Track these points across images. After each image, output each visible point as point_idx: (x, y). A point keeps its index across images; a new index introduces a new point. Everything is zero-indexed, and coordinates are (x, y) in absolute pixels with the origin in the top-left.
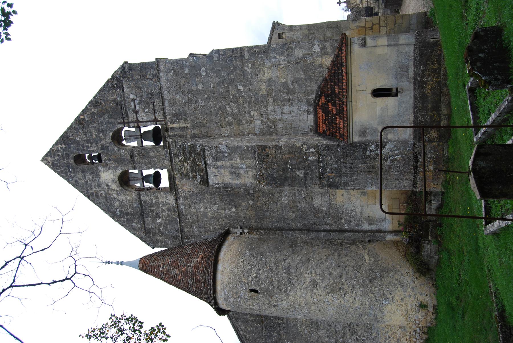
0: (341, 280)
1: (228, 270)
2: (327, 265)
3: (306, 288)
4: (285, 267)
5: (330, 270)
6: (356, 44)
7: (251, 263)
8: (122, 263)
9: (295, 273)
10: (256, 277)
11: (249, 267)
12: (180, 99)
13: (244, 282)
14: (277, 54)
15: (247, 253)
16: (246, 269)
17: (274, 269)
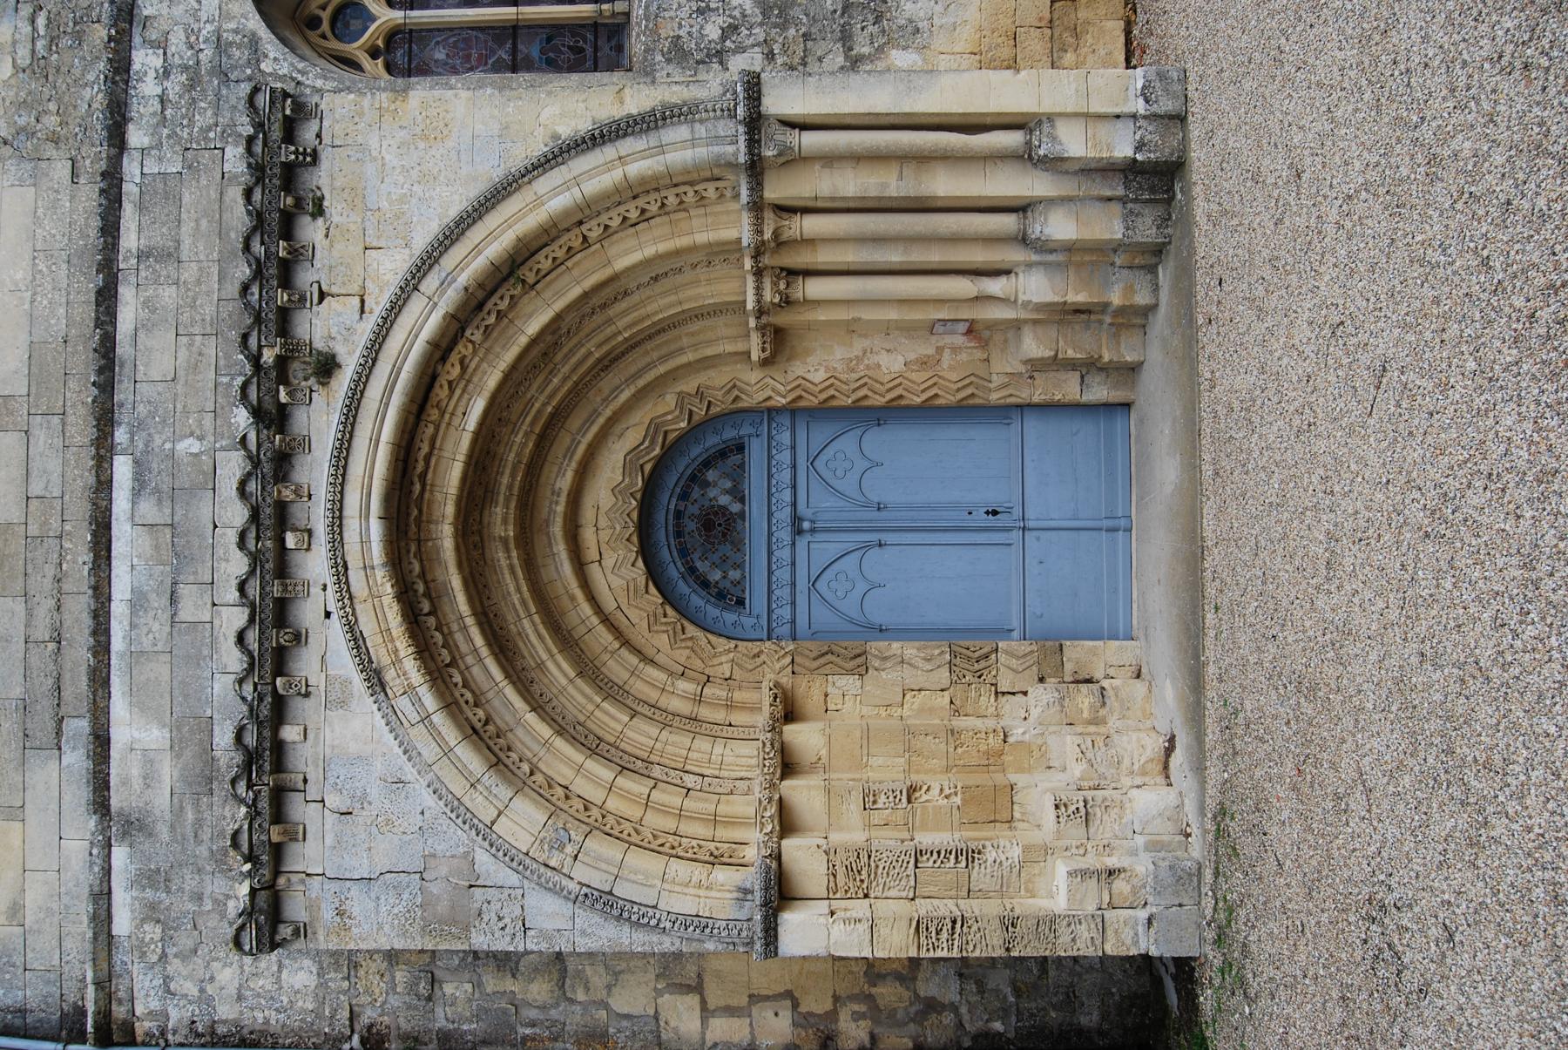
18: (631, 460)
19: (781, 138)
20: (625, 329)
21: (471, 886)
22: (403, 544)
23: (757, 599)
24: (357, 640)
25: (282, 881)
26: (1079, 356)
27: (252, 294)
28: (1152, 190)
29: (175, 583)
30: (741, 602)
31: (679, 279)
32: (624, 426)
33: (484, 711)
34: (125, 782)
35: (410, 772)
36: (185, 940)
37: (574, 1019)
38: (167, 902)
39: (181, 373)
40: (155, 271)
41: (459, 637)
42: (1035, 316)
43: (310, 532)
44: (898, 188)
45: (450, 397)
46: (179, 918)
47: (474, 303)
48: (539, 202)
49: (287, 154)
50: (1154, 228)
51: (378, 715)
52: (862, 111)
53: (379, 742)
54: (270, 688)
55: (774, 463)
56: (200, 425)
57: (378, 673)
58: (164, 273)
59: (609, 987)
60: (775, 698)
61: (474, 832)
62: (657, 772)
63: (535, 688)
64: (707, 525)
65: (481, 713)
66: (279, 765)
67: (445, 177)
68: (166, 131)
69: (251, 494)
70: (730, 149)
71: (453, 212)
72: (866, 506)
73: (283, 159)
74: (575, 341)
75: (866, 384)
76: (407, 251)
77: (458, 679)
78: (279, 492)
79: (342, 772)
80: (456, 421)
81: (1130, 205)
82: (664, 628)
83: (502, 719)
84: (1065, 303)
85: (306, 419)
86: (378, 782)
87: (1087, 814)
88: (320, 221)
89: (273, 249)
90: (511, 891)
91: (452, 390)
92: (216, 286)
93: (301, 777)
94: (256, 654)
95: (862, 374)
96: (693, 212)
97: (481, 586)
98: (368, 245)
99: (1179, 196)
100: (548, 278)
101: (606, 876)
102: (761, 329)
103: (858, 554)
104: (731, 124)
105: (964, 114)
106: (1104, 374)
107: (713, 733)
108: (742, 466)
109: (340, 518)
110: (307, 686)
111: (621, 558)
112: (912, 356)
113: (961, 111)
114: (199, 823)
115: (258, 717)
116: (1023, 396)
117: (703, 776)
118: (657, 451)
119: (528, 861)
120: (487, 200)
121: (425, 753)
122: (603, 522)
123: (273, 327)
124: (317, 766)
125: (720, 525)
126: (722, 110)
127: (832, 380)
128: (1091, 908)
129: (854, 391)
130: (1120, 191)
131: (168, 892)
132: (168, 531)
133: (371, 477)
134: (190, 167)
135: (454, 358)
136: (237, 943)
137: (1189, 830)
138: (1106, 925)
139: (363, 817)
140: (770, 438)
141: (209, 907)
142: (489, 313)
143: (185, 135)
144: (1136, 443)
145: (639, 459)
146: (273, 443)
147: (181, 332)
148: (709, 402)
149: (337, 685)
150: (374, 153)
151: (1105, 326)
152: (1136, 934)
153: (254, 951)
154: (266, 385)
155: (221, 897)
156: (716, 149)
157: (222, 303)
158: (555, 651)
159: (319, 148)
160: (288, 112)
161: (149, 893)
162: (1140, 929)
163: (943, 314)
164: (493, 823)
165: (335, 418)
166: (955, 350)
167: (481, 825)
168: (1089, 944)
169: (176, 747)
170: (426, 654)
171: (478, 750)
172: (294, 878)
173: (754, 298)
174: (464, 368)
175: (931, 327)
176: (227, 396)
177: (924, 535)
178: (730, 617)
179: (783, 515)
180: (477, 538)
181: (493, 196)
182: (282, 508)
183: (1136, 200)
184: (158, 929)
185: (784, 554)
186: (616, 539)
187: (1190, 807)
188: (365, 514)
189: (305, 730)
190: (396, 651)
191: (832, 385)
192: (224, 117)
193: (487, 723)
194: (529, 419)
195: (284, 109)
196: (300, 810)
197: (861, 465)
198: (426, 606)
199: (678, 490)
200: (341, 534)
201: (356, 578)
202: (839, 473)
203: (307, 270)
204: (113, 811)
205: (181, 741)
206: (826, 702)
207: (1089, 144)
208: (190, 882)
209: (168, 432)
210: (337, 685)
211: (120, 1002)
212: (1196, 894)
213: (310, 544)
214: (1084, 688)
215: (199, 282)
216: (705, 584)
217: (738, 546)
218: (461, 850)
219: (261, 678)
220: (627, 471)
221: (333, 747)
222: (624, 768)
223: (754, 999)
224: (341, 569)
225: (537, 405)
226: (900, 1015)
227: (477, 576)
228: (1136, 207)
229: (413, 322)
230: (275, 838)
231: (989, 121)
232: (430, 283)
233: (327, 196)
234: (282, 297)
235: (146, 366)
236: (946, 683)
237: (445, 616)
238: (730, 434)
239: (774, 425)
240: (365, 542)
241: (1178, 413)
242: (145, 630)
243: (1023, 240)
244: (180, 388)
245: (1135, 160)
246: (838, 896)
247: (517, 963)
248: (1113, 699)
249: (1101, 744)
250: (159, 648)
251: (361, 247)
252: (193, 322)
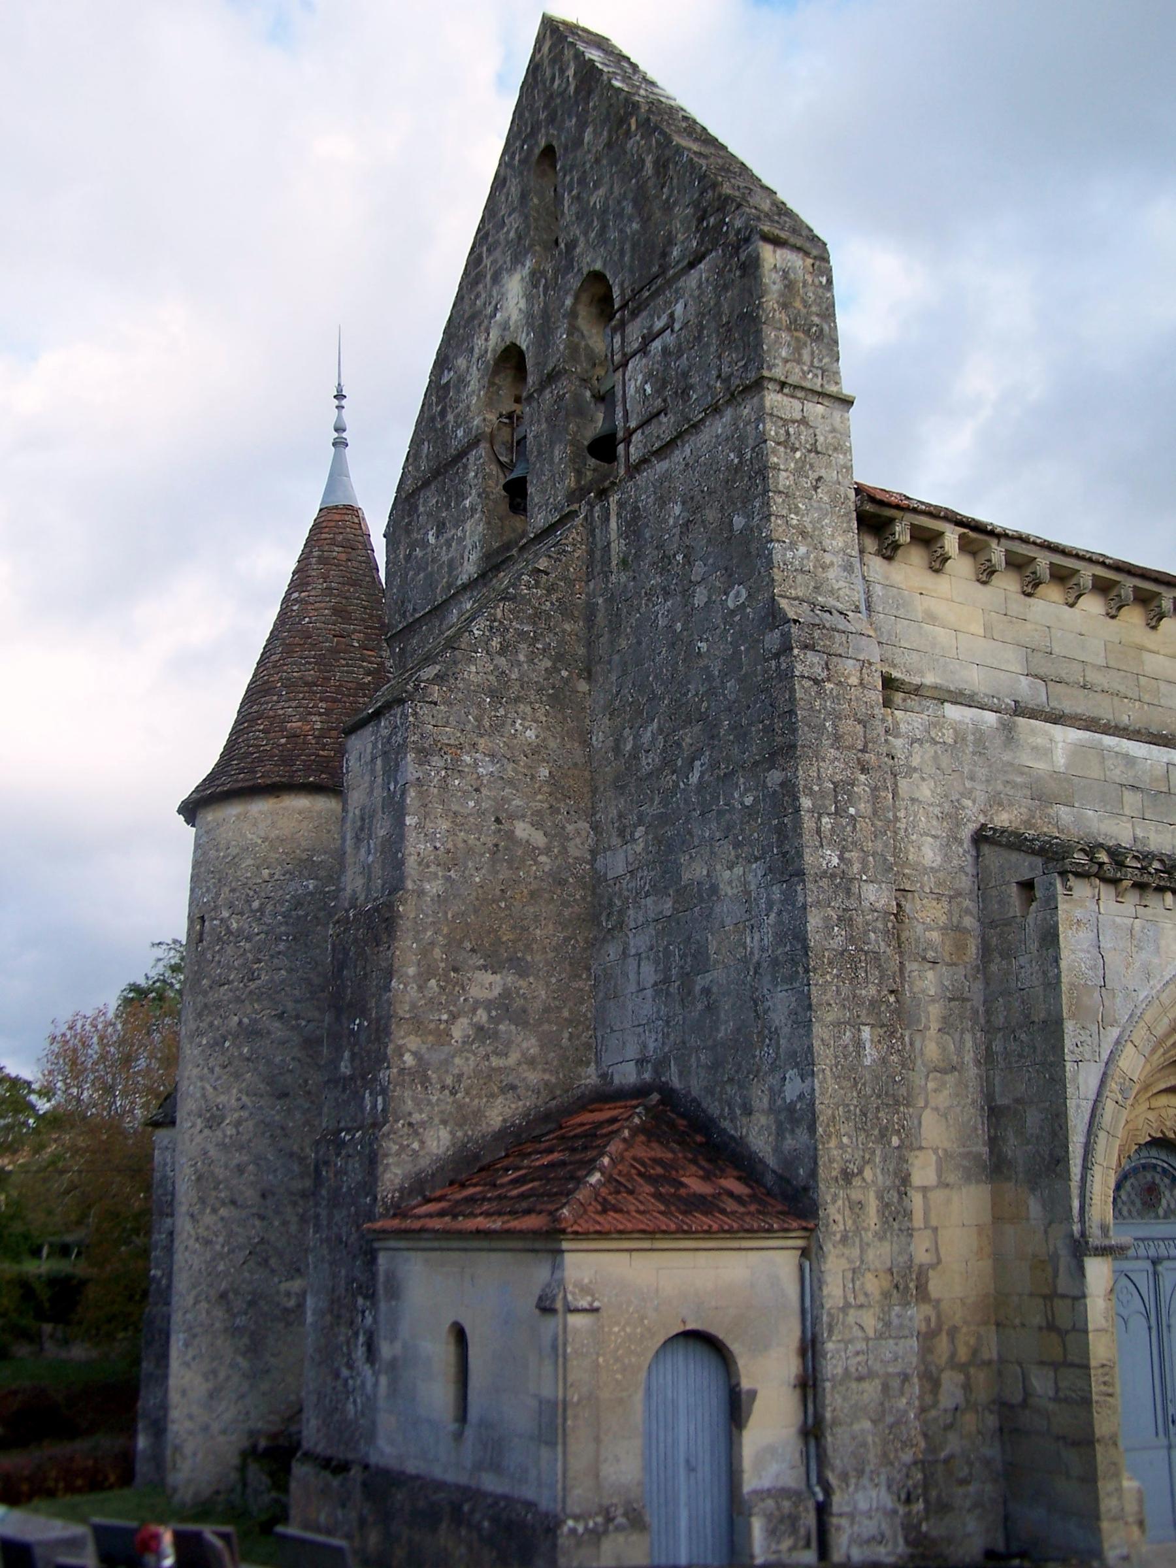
0: (223, 1204)
1: (249, 836)
2: (266, 1159)
3: (204, 1096)
4: (256, 1020)
5: (251, 1167)
6: (553, 1273)
7: (269, 908)
8: (340, 444)
9: (241, 1054)
10: (229, 932)
11: (256, 905)
12: (671, 521)
13: (218, 895)
14: (780, 913)
15: (307, 887)
16: (251, 893)
17: (252, 985)
34: (1033, 731)
37: (917, 1079)
59: (936, 1109)
114: (1015, 786)
161: (971, 738)
204: (1016, 718)
211: (904, 700)
223: (935, 1230)
226: (929, 1358)
247: (948, 1034)
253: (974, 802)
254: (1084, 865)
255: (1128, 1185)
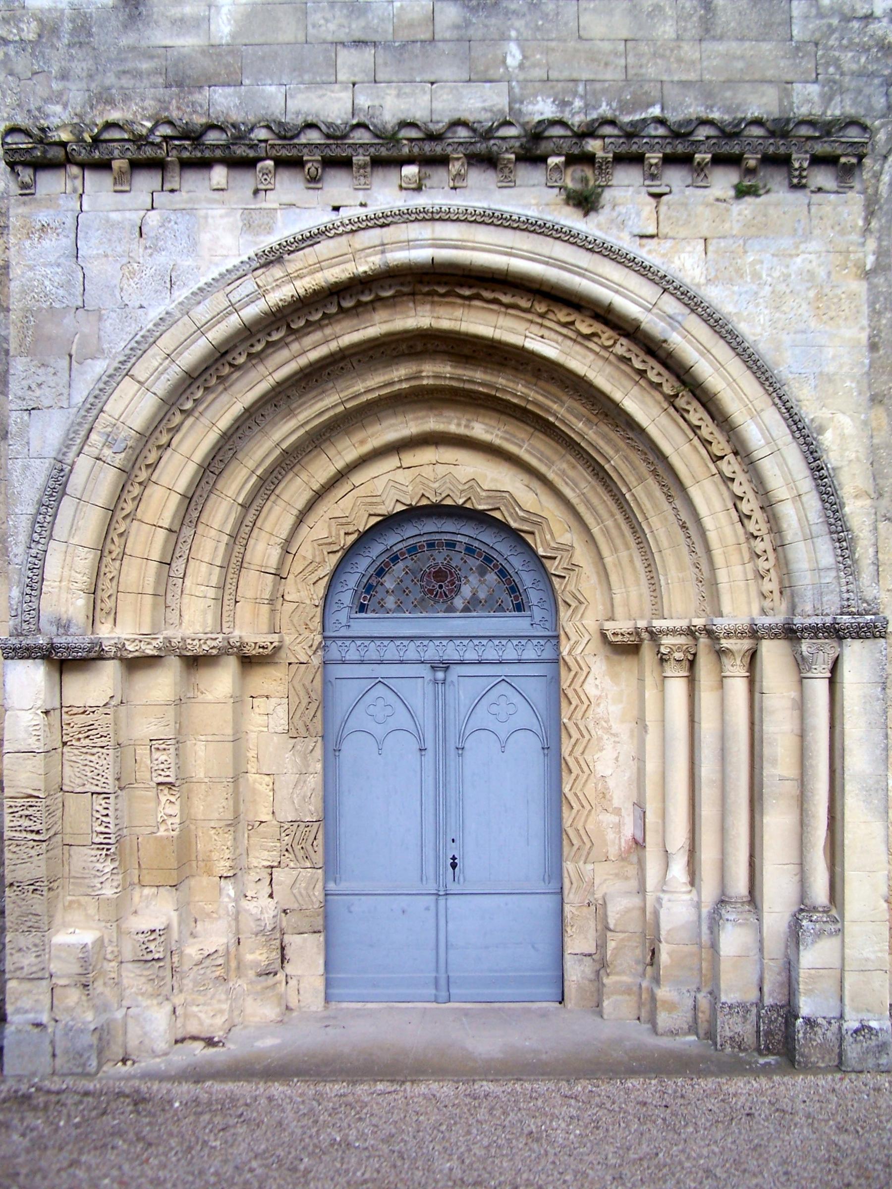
18: (503, 498)
19: (820, 660)
20: (633, 495)
21: (71, 356)
22: (409, 279)
23: (365, 625)
24: (310, 239)
25: (75, 170)
26: (609, 953)
27: (656, 129)
28: (768, 1033)
29: (375, 44)
30: (362, 608)
31: (685, 550)
32: (538, 492)
33: (244, 363)
35: (182, 294)
36: (21, 64)
38: (59, 45)
39: (587, 45)
40: (691, 16)
41: (317, 336)
42: (649, 910)
43: (419, 189)
44: (773, 776)
45: (559, 323)
46: (44, 57)
47: (652, 346)
48: (755, 415)
49: (800, 160)
50: (731, 1034)
51: (236, 261)
52: (846, 743)
53: (211, 262)
54: (263, 155)
55: (504, 642)
56: (534, 65)
57: (279, 260)
58: (689, 26)
60: (263, 647)
61: (122, 358)
62: (187, 532)
63: (269, 409)
64: (440, 575)
65: (241, 360)
66: (186, 165)
67: (779, 319)
68: (835, 22)
69: (455, 132)
70: (809, 608)
71: (743, 328)
72: (462, 737)
73: (794, 156)
74: (622, 444)
75: (583, 736)
76: (703, 281)
77: (275, 337)
78: (458, 159)
79: (182, 227)
80: (535, 329)
81: (754, 1010)
82: (334, 534)
83: (237, 379)
84: (660, 941)
85: (531, 182)
86: (172, 263)
87: (146, 961)
88: (732, 193)
89: (702, 148)
90: (66, 395)
91: (565, 325)
92: (676, 78)
93: (176, 187)
94: (296, 141)
95: (593, 732)
96: (749, 567)
97: (371, 353)
98: (709, 241)
99: (762, 1061)
100: (681, 421)
101: (80, 488)
102: (637, 632)
103: (412, 728)
104: (835, 608)
105: (843, 845)
106: (592, 976)
107: (228, 586)
108: (501, 608)
109: (433, 220)
110: (266, 190)
111: (404, 488)
112: (611, 783)
113: (846, 842)
114: (137, 74)
115: (233, 144)
116: (571, 896)
117: (183, 578)
118: (514, 525)
119: (94, 412)
120: (755, 362)
121: (201, 308)
122: (441, 470)
123: (623, 149)
124: (187, 202)
125: (441, 587)
126: (848, 599)
127: (586, 702)
128: (53, 967)
129: (576, 725)
130: (768, 1001)
131: (69, 46)
132: (427, 36)
133: (473, 249)
134: (797, 49)
135: (598, 327)
136: (13, 130)
137: (129, 1063)
138: (36, 982)
139: (138, 249)
140: (530, 638)
141: (54, 85)
142: (644, 361)
143: (831, 43)
144: (523, 1009)
145: (506, 506)
146: (507, 151)
147: (629, 44)
148: (564, 577)
149: (266, 220)
150: (802, 247)
151: (639, 980)
152: (26, 1012)
153: (6, 147)
154: (566, 145)
155: (65, 98)
156: (809, 593)
157: (659, 86)
158: (308, 428)
159: (807, 191)
160: (843, 160)
161: (67, 26)
162: (31, 1016)
163: (651, 818)
164: (132, 376)
165: (533, 214)
166: (618, 827)
167: (129, 365)
168: (17, 965)
169: (213, 50)
170: (300, 305)
171: (204, 359)
172: (78, 183)
173: (664, 627)
174: (588, 337)
175: (640, 807)
176: (565, 91)
177: (431, 793)
178: (347, 598)
179: (451, 652)
180: (419, 348)
181: (759, 368)
182: (443, 161)
183: (759, 1016)
184: (32, 36)
185: (411, 651)
186: (423, 484)
187: (146, 1063)
188: (437, 244)
189: (222, 190)
190: (300, 277)
191: (582, 702)
192: (851, 81)
193: (231, 365)
194: (541, 398)
195: (846, 155)
196: (146, 182)
197: (503, 731)
198: (347, 304)
199: (476, 544)
200: (416, 220)
201: (373, 236)
202: (494, 709)
203: (683, 181)
205: (219, 55)
206: (261, 696)
207: (813, 971)
208: (79, 67)
209: (528, 34)
210: (266, 220)
212: (65, 1070)
213: (406, 189)
214: (276, 955)
215: (680, 60)
216: (380, 572)
217: (420, 605)
218: (106, 346)
219: (273, 146)
220: (493, 494)
221: (206, 217)
222: (191, 499)
224: (382, 221)
225: (555, 407)
227: (382, 350)
228: (752, 1017)
229: (631, 288)
230: (116, 164)
231: (838, 869)
232: (670, 305)
233: (758, 200)
234: (654, 157)
235: (595, 10)
236: (281, 816)
237: (339, 321)
238: (534, 596)
239: (542, 642)
240: (409, 244)
241: (544, 1056)
242: (329, 16)
243: (723, 901)
244: (571, 44)
245: (796, 1017)
246: (65, 716)
248: (265, 984)
249: (218, 973)
250: (311, 30)
251: (708, 235)
252: (639, 56)
253: (65, 106)
254: (27, 150)
255: (399, 568)
